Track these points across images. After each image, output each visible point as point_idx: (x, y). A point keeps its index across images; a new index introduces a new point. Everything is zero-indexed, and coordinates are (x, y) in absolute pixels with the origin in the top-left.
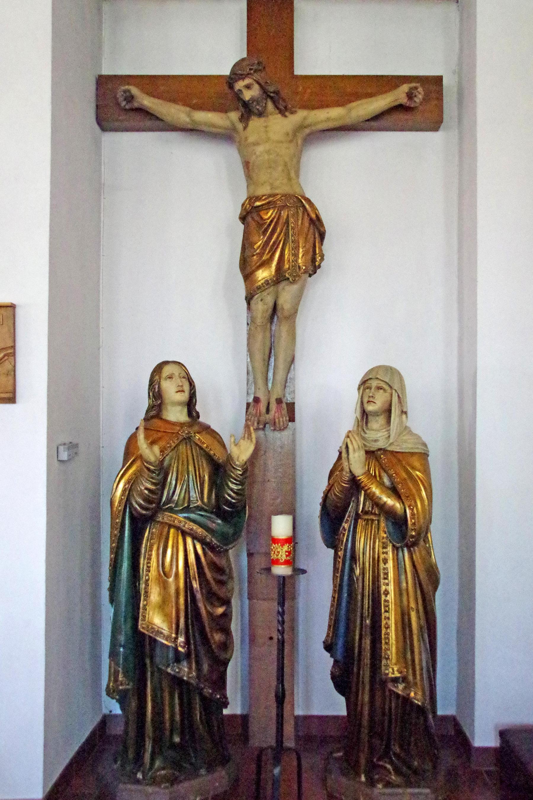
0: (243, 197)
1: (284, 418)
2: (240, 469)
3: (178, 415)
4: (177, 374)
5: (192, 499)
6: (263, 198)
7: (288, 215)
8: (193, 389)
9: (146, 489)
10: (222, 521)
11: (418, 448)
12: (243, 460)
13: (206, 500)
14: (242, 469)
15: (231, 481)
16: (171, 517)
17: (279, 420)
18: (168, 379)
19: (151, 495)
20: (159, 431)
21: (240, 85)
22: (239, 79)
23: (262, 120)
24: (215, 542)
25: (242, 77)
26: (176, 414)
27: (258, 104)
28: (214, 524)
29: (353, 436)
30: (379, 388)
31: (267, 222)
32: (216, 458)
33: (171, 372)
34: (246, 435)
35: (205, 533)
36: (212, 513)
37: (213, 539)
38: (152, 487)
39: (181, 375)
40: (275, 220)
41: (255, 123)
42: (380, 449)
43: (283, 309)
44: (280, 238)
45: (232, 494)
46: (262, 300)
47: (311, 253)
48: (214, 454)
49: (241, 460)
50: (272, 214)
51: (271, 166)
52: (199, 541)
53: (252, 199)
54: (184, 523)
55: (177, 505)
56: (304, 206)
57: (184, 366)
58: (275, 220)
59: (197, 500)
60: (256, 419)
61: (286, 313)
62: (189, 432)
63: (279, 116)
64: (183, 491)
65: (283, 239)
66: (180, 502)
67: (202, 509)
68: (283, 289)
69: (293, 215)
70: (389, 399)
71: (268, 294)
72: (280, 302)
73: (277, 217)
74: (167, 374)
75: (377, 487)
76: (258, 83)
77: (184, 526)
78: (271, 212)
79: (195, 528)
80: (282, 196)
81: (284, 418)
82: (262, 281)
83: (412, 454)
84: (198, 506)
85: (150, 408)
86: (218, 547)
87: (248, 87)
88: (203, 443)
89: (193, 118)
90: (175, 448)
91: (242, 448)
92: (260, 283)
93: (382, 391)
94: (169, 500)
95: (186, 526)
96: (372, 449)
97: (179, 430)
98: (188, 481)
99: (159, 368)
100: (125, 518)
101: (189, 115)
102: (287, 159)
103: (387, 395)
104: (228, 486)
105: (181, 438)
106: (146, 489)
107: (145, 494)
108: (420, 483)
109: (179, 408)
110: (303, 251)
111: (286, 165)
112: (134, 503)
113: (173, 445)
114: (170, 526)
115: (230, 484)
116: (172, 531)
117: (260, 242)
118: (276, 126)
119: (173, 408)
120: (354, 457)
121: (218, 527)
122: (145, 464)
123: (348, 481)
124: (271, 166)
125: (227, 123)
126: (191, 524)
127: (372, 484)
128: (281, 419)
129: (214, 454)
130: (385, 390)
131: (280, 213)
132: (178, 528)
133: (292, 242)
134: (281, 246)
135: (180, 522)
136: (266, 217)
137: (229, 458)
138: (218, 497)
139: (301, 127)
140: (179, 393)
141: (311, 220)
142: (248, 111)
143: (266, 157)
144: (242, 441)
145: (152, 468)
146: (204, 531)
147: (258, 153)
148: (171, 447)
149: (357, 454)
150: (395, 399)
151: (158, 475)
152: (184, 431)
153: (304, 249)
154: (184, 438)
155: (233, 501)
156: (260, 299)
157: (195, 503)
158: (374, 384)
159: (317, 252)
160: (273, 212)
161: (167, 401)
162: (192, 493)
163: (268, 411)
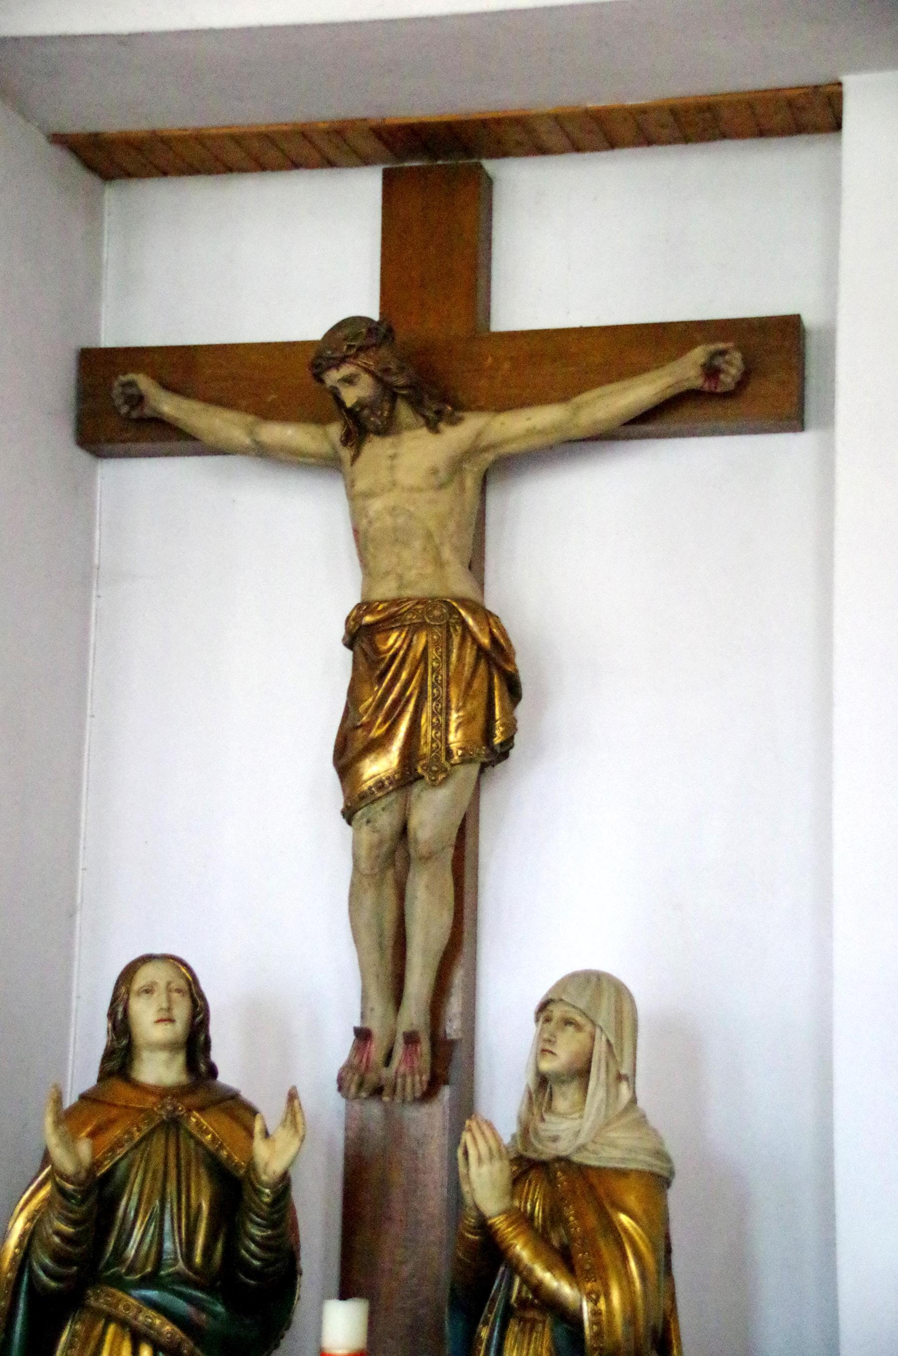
0: (355, 599)
1: (417, 1078)
2: (267, 1191)
4: (162, 984)
6: (380, 608)
7: (427, 642)
8: (199, 1014)
9: (58, 1233)
10: (227, 1309)
11: (634, 1160)
13: (198, 1259)
15: (252, 1221)
17: (405, 1081)
18: (145, 996)
21: (333, 377)
22: (329, 368)
23: (389, 440)
25: (338, 363)
26: (158, 1069)
27: (373, 413)
28: (204, 1316)
29: (480, 1128)
30: (568, 1022)
31: (383, 659)
33: (149, 979)
35: (180, 1334)
38: (68, 1230)
40: (401, 653)
41: (376, 449)
42: (559, 1159)
43: (416, 841)
44: (408, 693)
46: (368, 822)
47: (480, 720)
48: (229, 1157)
50: (396, 641)
51: (399, 537)
53: (365, 607)
56: (463, 622)
57: (185, 965)
58: (401, 653)
59: (176, 1259)
60: (356, 1077)
61: (423, 850)
63: (424, 431)
65: (416, 692)
66: (138, 1265)
67: (186, 1281)
68: (419, 796)
69: (436, 644)
70: (589, 1045)
71: (383, 809)
72: (413, 823)
73: (405, 646)
75: (525, 1245)
76: (367, 370)
77: (136, 1318)
78: (394, 636)
79: (158, 1322)
80: (417, 604)
81: (417, 1078)
82: (370, 783)
83: (622, 1174)
84: (178, 1273)
85: (109, 1055)
87: (349, 380)
88: (206, 1132)
89: (257, 439)
91: (279, 1145)
92: (365, 787)
93: (570, 1029)
95: (141, 1318)
96: (543, 1157)
97: (154, 1104)
98: (162, 1220)
101: (251, 433)
102: (432, 525)
103: (583, 1037)
105: (157, 1121)
108: (625, 1239)
109: (163, 1056)
110: (458, 718)
111: (429, 536)
112: (35, 1265)
113: (137, 1136)
114: (110, 1318)
116: (112, 1328)
117: (370, 700)
118: (416, 453)
120: (479, 1175)
122: (58, 1179)
123: (475, 1228)
124: (399, 537)
125: (325, 448)
126: (152, 1313)
127: (515, 1237)
128: (409, 1080)
129: (229, 1157)
130: (579, 1027)
131: (411, 641)
132: (123, 1323)
133: (433, 700)
134: (411, 707)
135: (127, 1308)
136: (385, 648)
137: (251, 1166)
138: (231, 1252)
139: (472, 452)
141: (480, 648)
142: (359, 428)
143: (389, 521)
144: (280, 1129)
145: (69, 1187)
146: (176, 1329)
147: (371, 513)
148: (131, 1139)
149: (485, 1169)
150: (600, 1048)
152: (163, 1107)
153: (461, 714)
155: (256, 1263)
156: (365, 820)
157: (174, 1265)
158: (557, 1012)
159: (497, 717)
160: (399, 636)
162: (168, 1245)
163: (388, 1059)
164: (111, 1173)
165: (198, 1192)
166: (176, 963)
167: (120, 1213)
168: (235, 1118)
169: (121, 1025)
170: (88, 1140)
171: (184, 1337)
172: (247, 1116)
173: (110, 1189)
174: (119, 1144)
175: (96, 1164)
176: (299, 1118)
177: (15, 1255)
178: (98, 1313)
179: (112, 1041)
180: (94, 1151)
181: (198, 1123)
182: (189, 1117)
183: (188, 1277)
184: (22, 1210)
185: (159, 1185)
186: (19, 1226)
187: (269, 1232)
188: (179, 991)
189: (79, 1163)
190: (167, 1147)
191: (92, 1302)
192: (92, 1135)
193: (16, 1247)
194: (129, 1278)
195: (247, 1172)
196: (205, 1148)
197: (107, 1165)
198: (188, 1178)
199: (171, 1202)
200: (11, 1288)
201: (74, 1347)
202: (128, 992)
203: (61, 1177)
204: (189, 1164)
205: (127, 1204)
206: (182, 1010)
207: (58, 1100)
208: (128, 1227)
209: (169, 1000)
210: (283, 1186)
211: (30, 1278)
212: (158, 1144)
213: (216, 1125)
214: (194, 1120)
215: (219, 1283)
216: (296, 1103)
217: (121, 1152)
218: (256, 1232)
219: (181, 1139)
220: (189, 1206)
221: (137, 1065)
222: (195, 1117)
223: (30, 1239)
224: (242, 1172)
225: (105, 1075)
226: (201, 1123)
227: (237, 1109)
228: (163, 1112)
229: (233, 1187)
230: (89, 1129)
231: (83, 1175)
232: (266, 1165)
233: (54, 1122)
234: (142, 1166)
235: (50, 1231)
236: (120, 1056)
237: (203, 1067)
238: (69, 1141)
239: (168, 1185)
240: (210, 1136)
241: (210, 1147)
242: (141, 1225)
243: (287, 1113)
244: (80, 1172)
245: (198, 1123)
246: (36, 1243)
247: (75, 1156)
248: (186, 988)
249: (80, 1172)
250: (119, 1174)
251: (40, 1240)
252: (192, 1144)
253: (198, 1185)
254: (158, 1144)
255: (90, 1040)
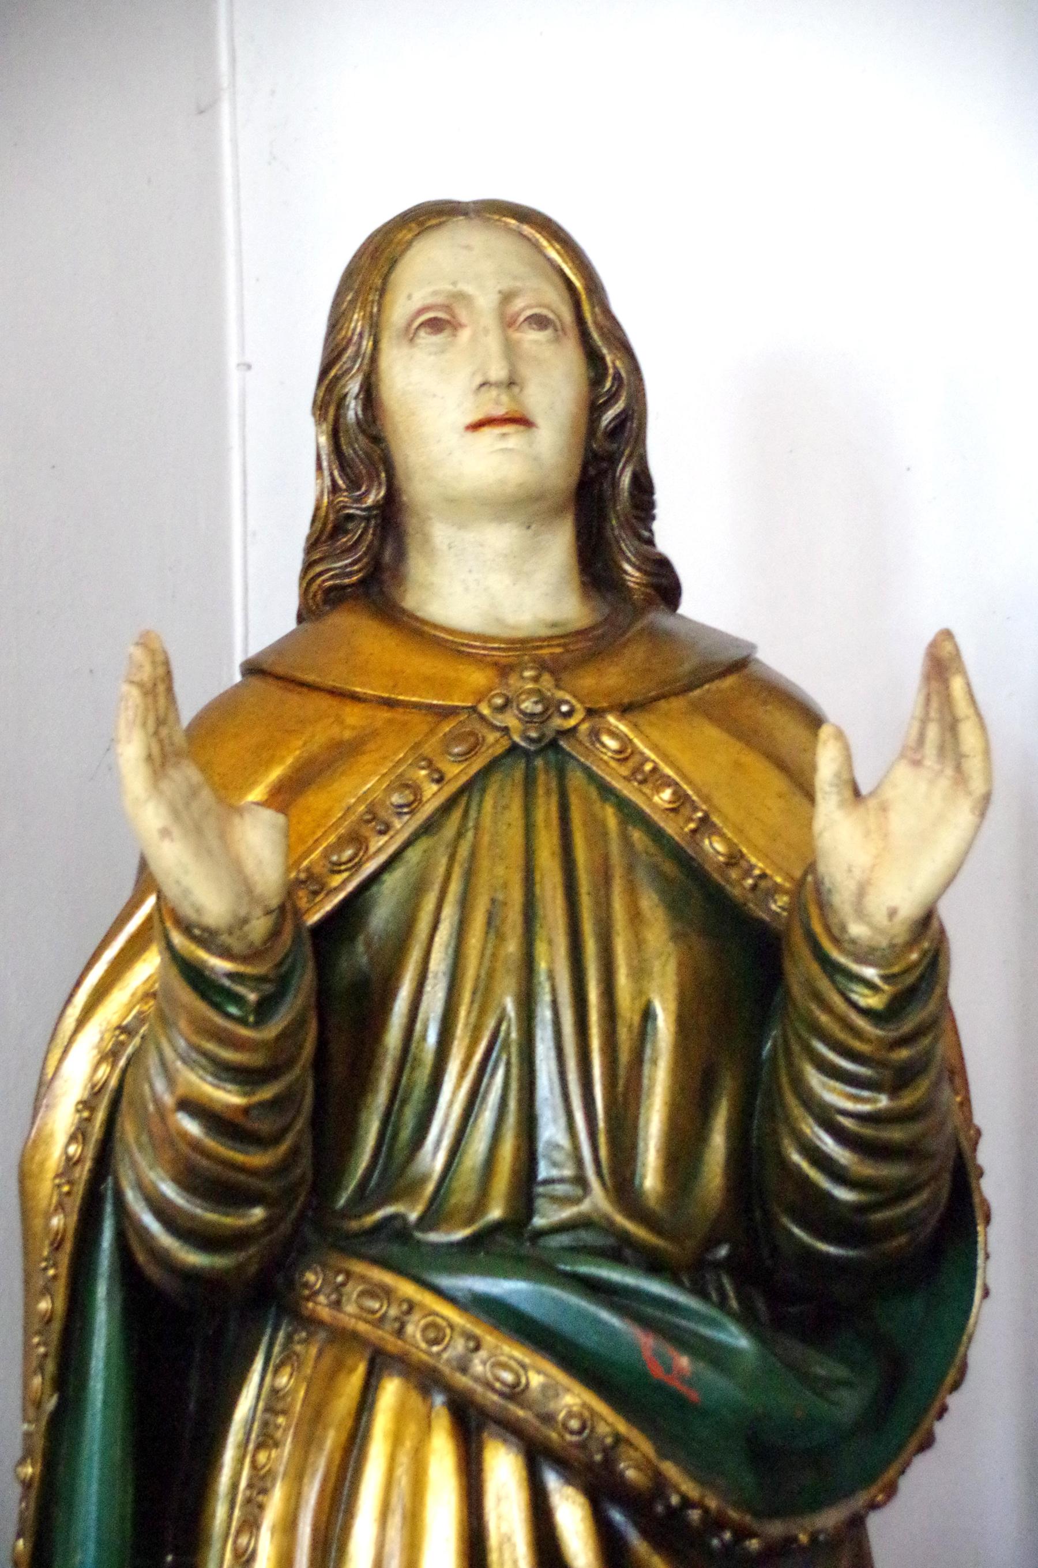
2: (870, 973)
3: (499, 582)
4: (486, 301)
5: (544, 1171)
8: (613, 398)
9: (189, 1105)
12: (892, 913)
13: (650, 1176)
14: (886, 978)
16: (386, 1293)
18: (425, 338)
19: (211, 1144)
20: (355, 698)
24: (690, 1488)
26: (489, 578)
32: (739, 887)
34: (933, 732)
35: (610, 1421)
36: (692, 1273)
37: (670, 1470)
38: (228, 1097)
39: (519, 304)
45: (829, 1144)
48: (735, 858)
49: (878, 904)
52: (573, 1471)
54: (459, 1346)
55: (431, 1218)
59: (580, 1180)
62: (550, 707)
64: (487, 1118)
66: (463, 1191)
74: (417, 303)
77: (464, 1368)
79: (536, 1380)
85: (328, 532)
86: (715, 1523)
88: (656, 779)
90: (446, 808)
91: (900, 821)
94: (394, 1171)
95: (478, 1367)
97: (482, 695)
99: (375, 264)
100: (91, 1292)
104: (799, 1084)
105: (494, 744)
106: (189, 1105)
107: (184, 1135)
109: (501, 538)
112: (132, 1197)
114: (380, 1364)
115: (815, 1079)
116: (391, 1391)
119: (470, 536)
121: (720, 1386)
122: (178, 939)
126: (514, 1352)
129: (735, 858)
135: (436, 1334)
137: (810, 889)
138: (750, 1158)
140: (489, 434)
144: (903, 772)
145: (219, 965)
146: (601, 1407)
151: (264, 1010)
154: (514, 748)
155: (843, 1194)
157: (578, 1201)
161: (420, 488)
162: (551, 1130)
164: (351, 912)
165: (640, 973)
166: (527, 229)
167: (393, 1037)
168: (748, 735)
169: (359, 442)
170: (268, 815)
171: (622, 1427)
172: (786, 729)
173: (359, 955)
174: (375, 819)
175: (307, 883)
176: (969, 737)
177: (71, 1163)
178: (342, 1338)
179: (335, 489)
180: (292, 845)
181: (625, 753)
182: (595, 734)
183: (625, 1238)
184: (81, 1022)
185: (512, 947)
186: (78, 1072)
187: (883, 1102)
188: (540, 322)
189: (246, 888)
190: (528, 811)
191: (321, 1307)
192: (284, 797)
193: (72, 1138)
194: (434, 1237)
195: (798, 907)
196: (656, 834)
197: (342, 887)
198: (603, 906)
199: (551, 977)
200: (64, 1258)
201: (276, 1445)
202: (375, 327)
203: (187, 928)
204: (604, 878)
205: (419, 1003)
206: (554, 388)
207: (160, 687)
208: (423, 1075)
209: (510, 350)
210: (922, 964)
211: (120, 1236)
212: (500, 814)
213: (685, 760)
214: (613, 744)
215: (723, 1251)
216: (957, 684)
217: (381, 847)
218: (833, 1094)
219: (574, 801)
220: (610, 1014)
221: (417, 566)
222: (614, 734)
223: (111, 1111)
224: (779, 904)
225: (319, 601)
226: (635, 751)
227: (750, 704)
228: (510, 720)
229: (752, 958)
230: (276, 773)
231: (259, 927)
232: (861, 892)
233: (149, 758)
234: (455, 888)
235: (169, 1100)
236: (364, 540)
237: (632, 574)
238: (208, 821)
239: (541, 949)
240: (667, 794)
241: (670, 828)
242: (462, 1075)
243: (924, 722)
244: (245, 921)
245: (625, 753)
246: (128, 1128)
247: (237, 865)
248: (567, 316)
249: (245, 921)
250: (382, 915)
251: (143, 1122)
252: (610, 816)
253: (638, 944)
254: (500, 814)
255: (275, 487)
